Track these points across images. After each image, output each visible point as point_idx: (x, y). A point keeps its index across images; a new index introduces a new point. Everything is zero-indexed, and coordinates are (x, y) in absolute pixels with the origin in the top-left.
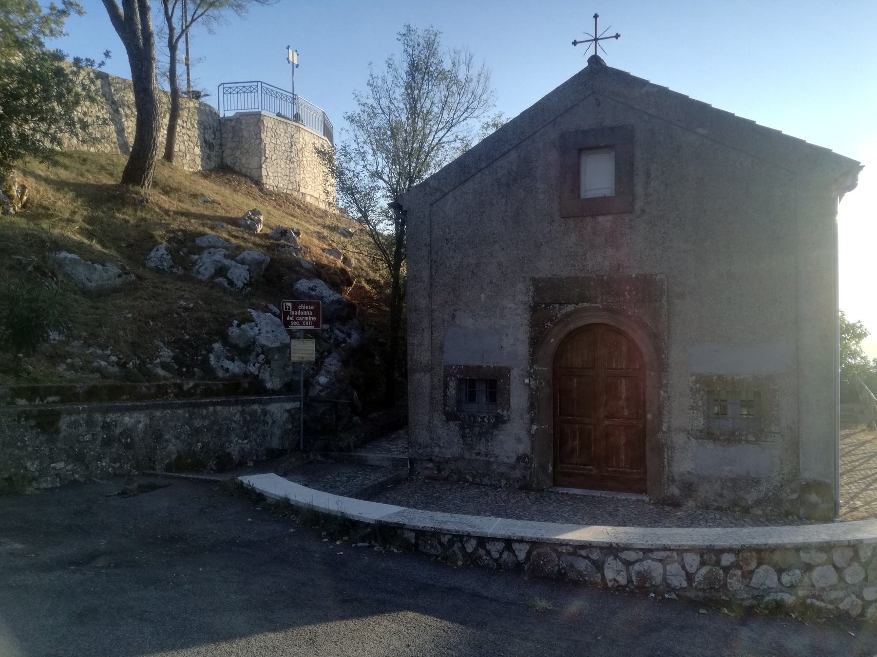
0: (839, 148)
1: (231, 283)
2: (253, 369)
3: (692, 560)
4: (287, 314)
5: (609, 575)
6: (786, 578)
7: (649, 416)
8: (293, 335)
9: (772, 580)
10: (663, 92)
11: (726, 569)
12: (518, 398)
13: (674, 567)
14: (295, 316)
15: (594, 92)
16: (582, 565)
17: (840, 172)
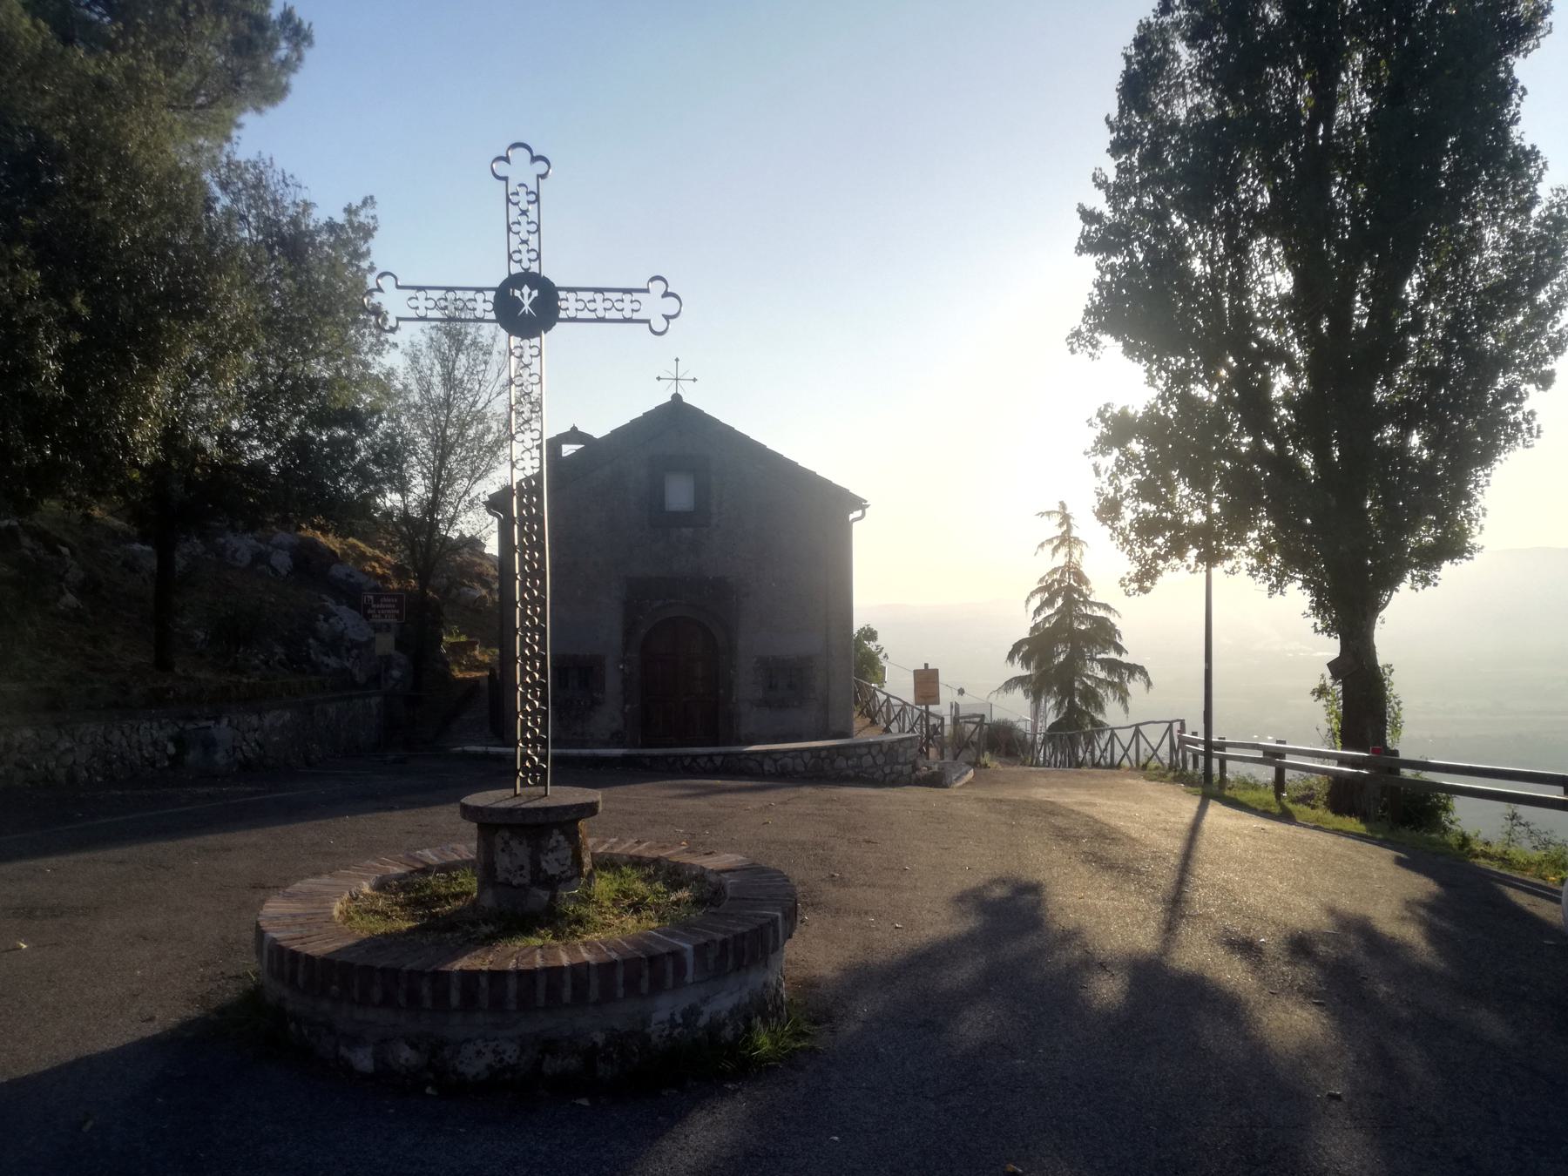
1: (275, 570)
2: (348, 664)
3: (807, 756)
4: (368, 606)
5: (766, 768)
8: (377, 629)
9: (844, 764)
10: (730, 431)
12: (612, 682)
13: (798, 761)
15: (1291, 986)
16: (751, 764)
17: (859, 504)
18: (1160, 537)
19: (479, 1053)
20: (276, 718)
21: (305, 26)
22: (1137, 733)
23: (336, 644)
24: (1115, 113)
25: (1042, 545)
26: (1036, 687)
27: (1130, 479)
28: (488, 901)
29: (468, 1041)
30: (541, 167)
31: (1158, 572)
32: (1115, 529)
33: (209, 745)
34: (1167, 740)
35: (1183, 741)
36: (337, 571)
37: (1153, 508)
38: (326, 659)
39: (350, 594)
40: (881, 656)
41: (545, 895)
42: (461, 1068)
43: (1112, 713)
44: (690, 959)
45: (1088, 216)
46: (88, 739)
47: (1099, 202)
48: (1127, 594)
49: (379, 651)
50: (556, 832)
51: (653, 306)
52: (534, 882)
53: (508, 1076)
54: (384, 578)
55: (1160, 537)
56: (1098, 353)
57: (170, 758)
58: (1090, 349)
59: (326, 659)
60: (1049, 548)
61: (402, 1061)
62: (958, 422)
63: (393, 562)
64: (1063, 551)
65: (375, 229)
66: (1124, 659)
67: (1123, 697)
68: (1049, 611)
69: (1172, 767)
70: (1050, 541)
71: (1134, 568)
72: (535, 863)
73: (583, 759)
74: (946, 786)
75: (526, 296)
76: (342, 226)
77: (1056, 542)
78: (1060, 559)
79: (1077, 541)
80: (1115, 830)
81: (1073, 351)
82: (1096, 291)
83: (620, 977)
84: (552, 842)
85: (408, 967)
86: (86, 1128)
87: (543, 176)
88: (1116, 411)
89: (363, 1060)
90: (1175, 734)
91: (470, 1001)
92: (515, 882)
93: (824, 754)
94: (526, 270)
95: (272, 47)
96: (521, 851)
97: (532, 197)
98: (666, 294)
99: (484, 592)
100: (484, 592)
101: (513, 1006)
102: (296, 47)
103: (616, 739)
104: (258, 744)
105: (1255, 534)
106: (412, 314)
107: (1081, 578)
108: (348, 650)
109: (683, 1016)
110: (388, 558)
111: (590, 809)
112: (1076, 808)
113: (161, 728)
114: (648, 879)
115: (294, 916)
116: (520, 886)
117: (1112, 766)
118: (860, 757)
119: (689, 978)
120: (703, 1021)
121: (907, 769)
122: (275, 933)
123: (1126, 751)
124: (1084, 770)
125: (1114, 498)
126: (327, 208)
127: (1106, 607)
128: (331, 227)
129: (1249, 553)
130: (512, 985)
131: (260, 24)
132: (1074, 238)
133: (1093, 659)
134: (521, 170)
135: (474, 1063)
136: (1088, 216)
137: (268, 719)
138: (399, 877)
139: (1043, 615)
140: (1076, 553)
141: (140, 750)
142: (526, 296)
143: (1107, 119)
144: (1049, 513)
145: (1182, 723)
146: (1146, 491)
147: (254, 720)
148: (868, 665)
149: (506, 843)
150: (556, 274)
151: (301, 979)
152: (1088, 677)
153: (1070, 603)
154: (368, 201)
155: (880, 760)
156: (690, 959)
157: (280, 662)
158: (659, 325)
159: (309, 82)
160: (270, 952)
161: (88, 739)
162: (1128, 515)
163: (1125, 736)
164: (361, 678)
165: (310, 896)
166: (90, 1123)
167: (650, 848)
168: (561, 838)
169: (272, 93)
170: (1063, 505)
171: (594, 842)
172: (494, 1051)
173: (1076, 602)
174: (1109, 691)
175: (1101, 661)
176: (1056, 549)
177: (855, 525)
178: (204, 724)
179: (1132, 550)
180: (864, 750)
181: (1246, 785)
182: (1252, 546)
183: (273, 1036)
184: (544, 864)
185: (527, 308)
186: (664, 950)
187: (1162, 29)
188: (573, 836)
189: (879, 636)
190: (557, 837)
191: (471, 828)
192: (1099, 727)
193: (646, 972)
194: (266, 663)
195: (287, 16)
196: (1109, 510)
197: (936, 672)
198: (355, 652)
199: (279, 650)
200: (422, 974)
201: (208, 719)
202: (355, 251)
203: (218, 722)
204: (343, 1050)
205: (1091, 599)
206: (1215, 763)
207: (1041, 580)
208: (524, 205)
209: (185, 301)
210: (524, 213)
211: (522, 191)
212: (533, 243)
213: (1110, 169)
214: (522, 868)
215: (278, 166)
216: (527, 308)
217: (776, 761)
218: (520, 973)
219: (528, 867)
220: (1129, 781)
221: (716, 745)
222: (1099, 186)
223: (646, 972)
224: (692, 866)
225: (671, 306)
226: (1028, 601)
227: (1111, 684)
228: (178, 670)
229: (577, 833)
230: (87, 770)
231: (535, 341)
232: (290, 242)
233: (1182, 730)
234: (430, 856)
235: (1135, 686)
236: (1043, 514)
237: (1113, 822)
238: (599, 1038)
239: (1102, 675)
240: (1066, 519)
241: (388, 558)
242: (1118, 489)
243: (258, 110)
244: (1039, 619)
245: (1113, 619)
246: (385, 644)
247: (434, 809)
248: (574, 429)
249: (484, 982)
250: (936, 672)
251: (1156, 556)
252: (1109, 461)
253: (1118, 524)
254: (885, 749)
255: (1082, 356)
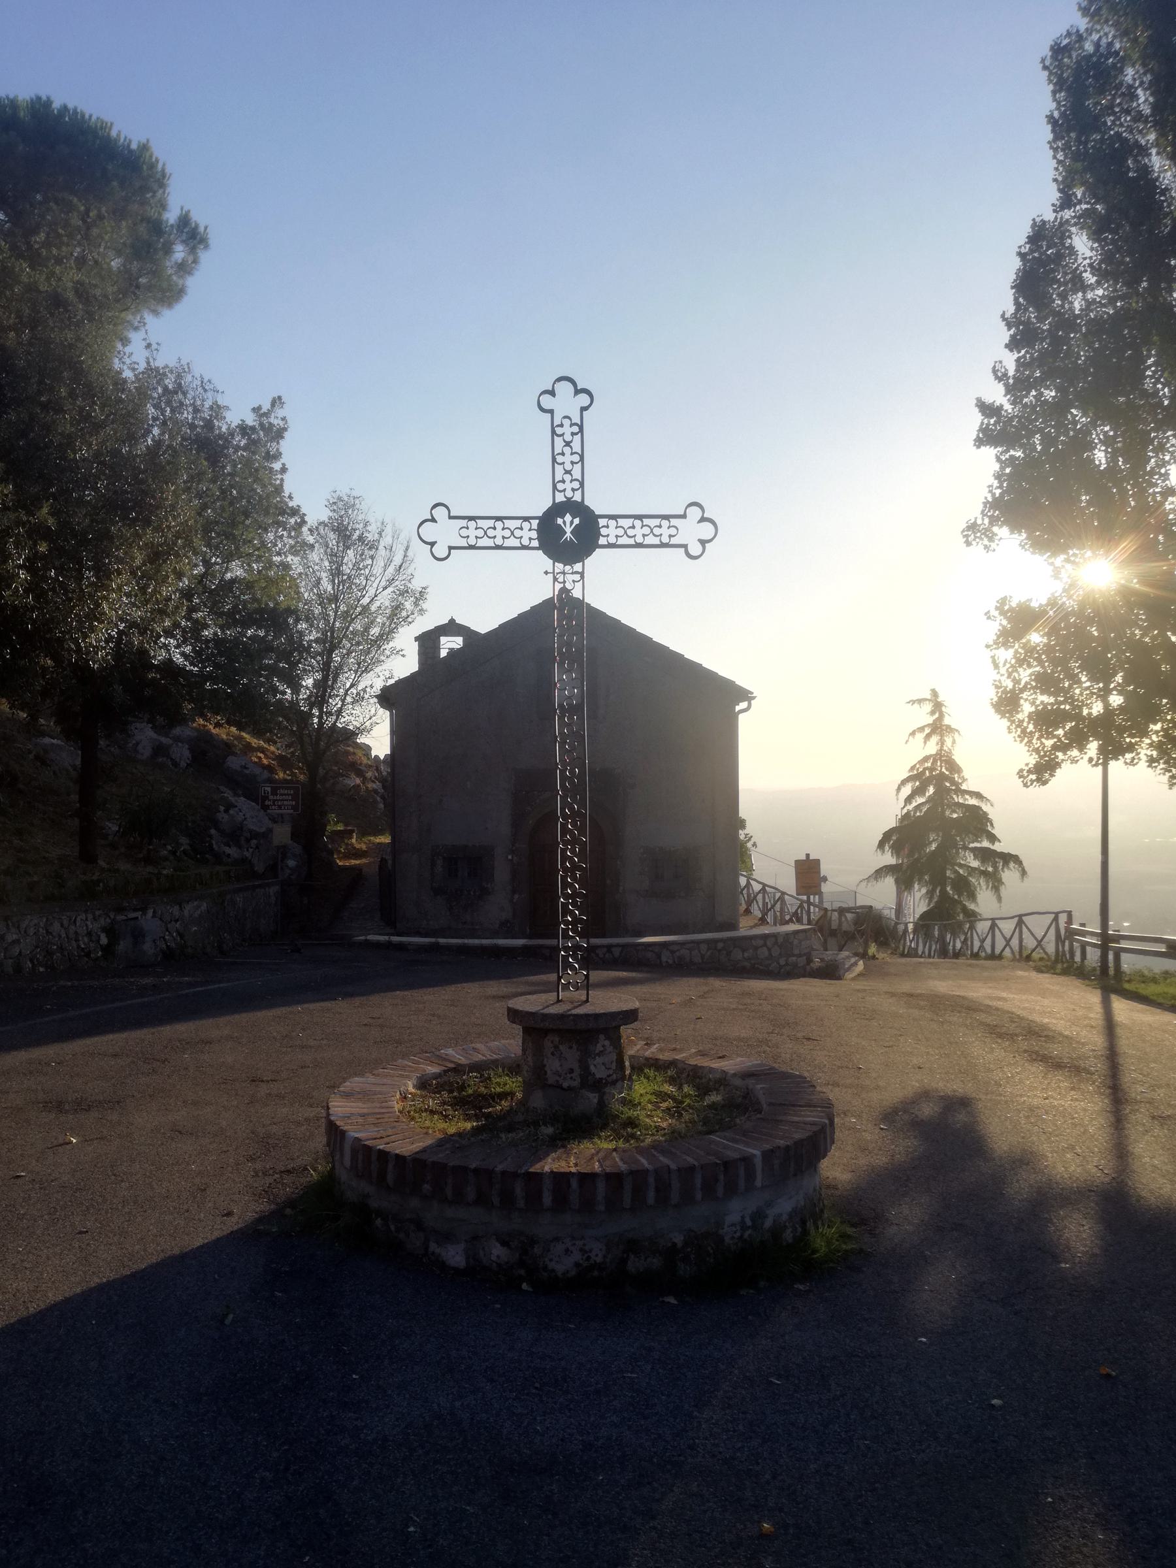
0: (741, 681)
1: (176, 764)
3: (703, 947)
4: (266, 798)
5: (664, 959)
6: (746, 955)
7: (608, 882)
9: (740, 957)
10: (616, 623)
11: (720, 951)
12: (501, 874)
14: (274, 801)
17: (745, 695)
18: (1060, 730)
19: (567, 1251)
20: (195, 909)
21: (202, 229)
22: (1020, 923)
23: (235, 835)
24: (1011, 309)
25: (913, 733)
26: (904, 877)
27: (1029, 671)
28: (538, 1101)
29: (557, 1239)
30: (584, 400)
31: (1058, 765)
32: (1013, 722)
33: (138, 936)
34: (1052, 931)
35: (1071, 933)
36: (234, 763)
37: (1052, 700)
38: (228, 850)
39: (247, 785)
40: (749, 845)
41: (594, 1098)
42: (551, 1265)
43: (985, 902)
44: (758, 1163)
45: (987, 409)
46: (32, 931)
47: (997, 395)
48: (1025, 785)
49: (276, 841)
50: (602, 1037)
51: (690, 531)
52: (584, 1085)
53: (596, 1273)
54: (269, 768)
55: (1060, 730)
56: (993, 545)
57: (103, 948)
58: (986, 542)
59: (228, 850)
60: (920, 736)
61: (494, 1258)
62: (852, 619)
63: (278, 752)
64: (935, 739)
65: (285, 429)
66: (997, 847)
67: (996, 883)
68: (920, 800)
69: (1059, 957)
70: (921, 729)
71: (1032, 760)
72: (585, 1067)
73: (484, 949)
74: (839, 978)
75: (568, 524)
76: (253, 428)
77: (927, 731)
78: (932, 748)
79: (949, 729)
80: (1044, 1027)
81: (968, 544)
82: (996, 483)
83: (698, 1182)
84: (599, 1048)
85: (500, 1168)
86: (228, 1321)
87: (583, 409)
88: (1014, 605)
89: (454, 1255)
90: (1062, 925)
91: (561, 1202)
92: (565, 1085)
93: (720, 945)
94: (569, 499)
95: (168, 250)
96: (571, 1055)
97: (576, 429)
98: (703, 519)
99: (358, 781)
100: (358, 781)
101: (602, 1208)
102: (193, 250)
103: (506, 929)
104: (179, 933)
105: (1158, 727)
106: (463, 543)
107: (953, 767)
108: (248, 840)
109: (752, 1220)
110: (272, 748)
111: (630, 1016)
112: (988, 1002)
113: (95, 919)
114: (672, 1081)
115: (363, 1115)
116: (570, 1089)
117: (993, 957)
118: (756, 948)
119: (758, 1183)
120: (768, 1223)
121: (802, 961)
122: (355, 1132)
123: (1008, 942)
124: (961, 961)
125: (1013, 691)
126: (238, 413)
127: (978, 795)
128: (244, 429)
129: (1151, 745)
130: (601, 1187)
131: (157, 227)
132: (973, 431)
133: (965, 848)
134: (566, 403)
135: (562, 1263)
136: (987, 409)
137: (188, 909)
138: (437, 1076)
139: (914, 804)
140: (948, 741)
141: (77, 940)
142: (568, 524)
143: (1003, 316)
144: (920, 701)
145: (1070, 914)
146: (1044, 683)
147: (175, 910)
148: (737, 853)
149: (556, 1047)
150: (597, 503)
151: (390, 1178)
152: (961, 866)
153: (942, 792)
154: (277, 402)
155: (776, 952)
156: (758, 1163)
157: (184, 852)
158: (695, 549)
159: (207, 283)
160: (354, 1152)
161: (32, 931)
162: (1027, 708)
163: (1007, 927)
164: (259, 867)
165: (364, 1095)
166: (231, 1316)
167: (661, 1050)
168: (607, 1043)
169: (167, 294)
170: (935, 693)
171: (634, 1046)
172: (581, 1250)
173: (948, 790)
174: (982, 881)
175: (974, 850)
176: (928, 737)
177: (741, 716)
178: (132, 915)
179: (1030, 742)
180: (760, 942)
181: (1144, 979)
182: (1154, 738)
183: (342, 1228)
184: (592, 1068)
185: (568, 535)
186: (736, 1156)
187: (1064, 223)
188: (616, 1041)
189: (748, 824)
190: (603, 1042)
191: (518, 1030)
192: (972, 916)
193: (721, 1177)
194: (174, 853)
195: (185, 220)
196: (1007, 703)
197: (817, 862)
198: (254, 842)
199: (184, 840)
200: (515, 1175)
201: (135, 910)
202: (268, 452)
203: (144, 913)
204: (433, 1247)
205: (964, 787)
206: (1111, 956)
207: (912, 768)
208: (568, 440)
209: (132, 509)
210: (568, 444)
211: (567, 422)
212: (577, 473)
213: (1010, 361)
214: (572, 1071)
215: (197, 372)
216: (568, 535)
217: (673, 952)
218: (608, 1176)
219: (577, 1071)
220: (1020, 973)
221: (604, 936)
222: (999, 379)
223: (721, 1177)
224: (711, 1070)
225: (707, 531)
226: (899, 789)
227: (985, 873)
228: (102, 863)
229: (619, 1037)
230: (31, 961)
231: (578, 567)
232: (208, 444)
233: (1070, 921)
234: (455, 1055)
235: (1009, 876)
236: (913, 702)
237: (1037, 1018)
238: (678, 1239)
239: (975, 864)
240: (938, 707)
241: (272, 748)
242: (1016, 682)
243: (156, 313)
244: (910, 807)
245: (985, 808)
246: (282, 834)
247: (375, 999)
248: (452, 621)
249: (574, 1183)
250: (817, 862)
251: (1055, 748)
252: (1006, 655)
253: (1020, 716)
254: (780, 940)
255: (977, 549)
